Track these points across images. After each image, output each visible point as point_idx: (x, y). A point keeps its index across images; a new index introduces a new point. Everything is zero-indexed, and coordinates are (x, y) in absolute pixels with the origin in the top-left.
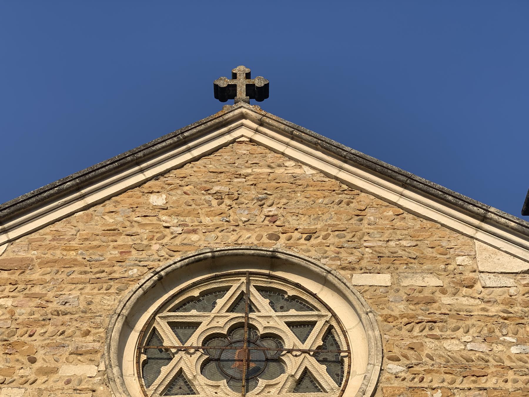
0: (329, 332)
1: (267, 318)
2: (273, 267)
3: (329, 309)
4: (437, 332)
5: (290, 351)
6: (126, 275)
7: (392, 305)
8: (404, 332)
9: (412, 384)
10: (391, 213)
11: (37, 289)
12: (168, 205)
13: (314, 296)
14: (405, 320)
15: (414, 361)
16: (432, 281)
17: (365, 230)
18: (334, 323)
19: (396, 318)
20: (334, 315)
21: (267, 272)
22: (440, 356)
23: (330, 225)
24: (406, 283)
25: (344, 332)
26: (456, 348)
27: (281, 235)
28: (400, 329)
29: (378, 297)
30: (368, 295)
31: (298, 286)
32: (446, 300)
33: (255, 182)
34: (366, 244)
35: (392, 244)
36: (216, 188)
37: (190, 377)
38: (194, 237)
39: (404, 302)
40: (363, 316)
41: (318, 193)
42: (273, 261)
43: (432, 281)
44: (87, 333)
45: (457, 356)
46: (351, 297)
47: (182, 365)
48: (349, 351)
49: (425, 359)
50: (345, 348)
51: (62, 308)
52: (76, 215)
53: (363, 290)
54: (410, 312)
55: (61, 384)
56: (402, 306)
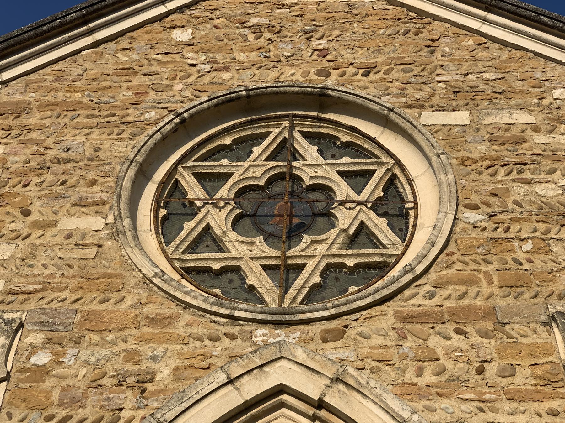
0: (391, 183)
1: (313, 165)
2: (323, 108)
3: (392, 155)
4: (527, 175)
5: (342, 203)
6: (141, 118)
7: (471, 146)
8: (485, 176)
9: (495, 235)
10: (471, 42)
11: (34, 135)
12: (194, 41)
13: (373, 140)
14: (487, 163)
15: (497, 209)
16: (523, 118)
17: (437, 63)
18: (397, 172)
19: (475, 161)
20: (398, 162)
21: (315, 114)
22: (531, 203)
23: (393, 59)
24: (488, 120)
25: (410, 181)
26: (552, 193)
27: (332, 71)
28: (480, 173)
29: (453, 138)
30: (440, 136)
31: (353, 129)
32: (540, 139)
33: (301, 13)
34: (438, 78)
35: (472, 77)
36: (254, 21)
37: (219, 233)
38: (226, 75)
39: (486, 143)
40: (434, 159)
41: (380, 23)
42: (322, 100)
43: (523, 118)
44: (93, 183)
45: (553, 202)
46: (419, 138)
47: (209, 220)
48: (415, 202)
49: (511, 206)
50: (411, 198)
51: (64, 155)
52: (84, 53)
53: (435, 130)
54: (493, 153)
55: (59, 239)
56: (484, 147)
